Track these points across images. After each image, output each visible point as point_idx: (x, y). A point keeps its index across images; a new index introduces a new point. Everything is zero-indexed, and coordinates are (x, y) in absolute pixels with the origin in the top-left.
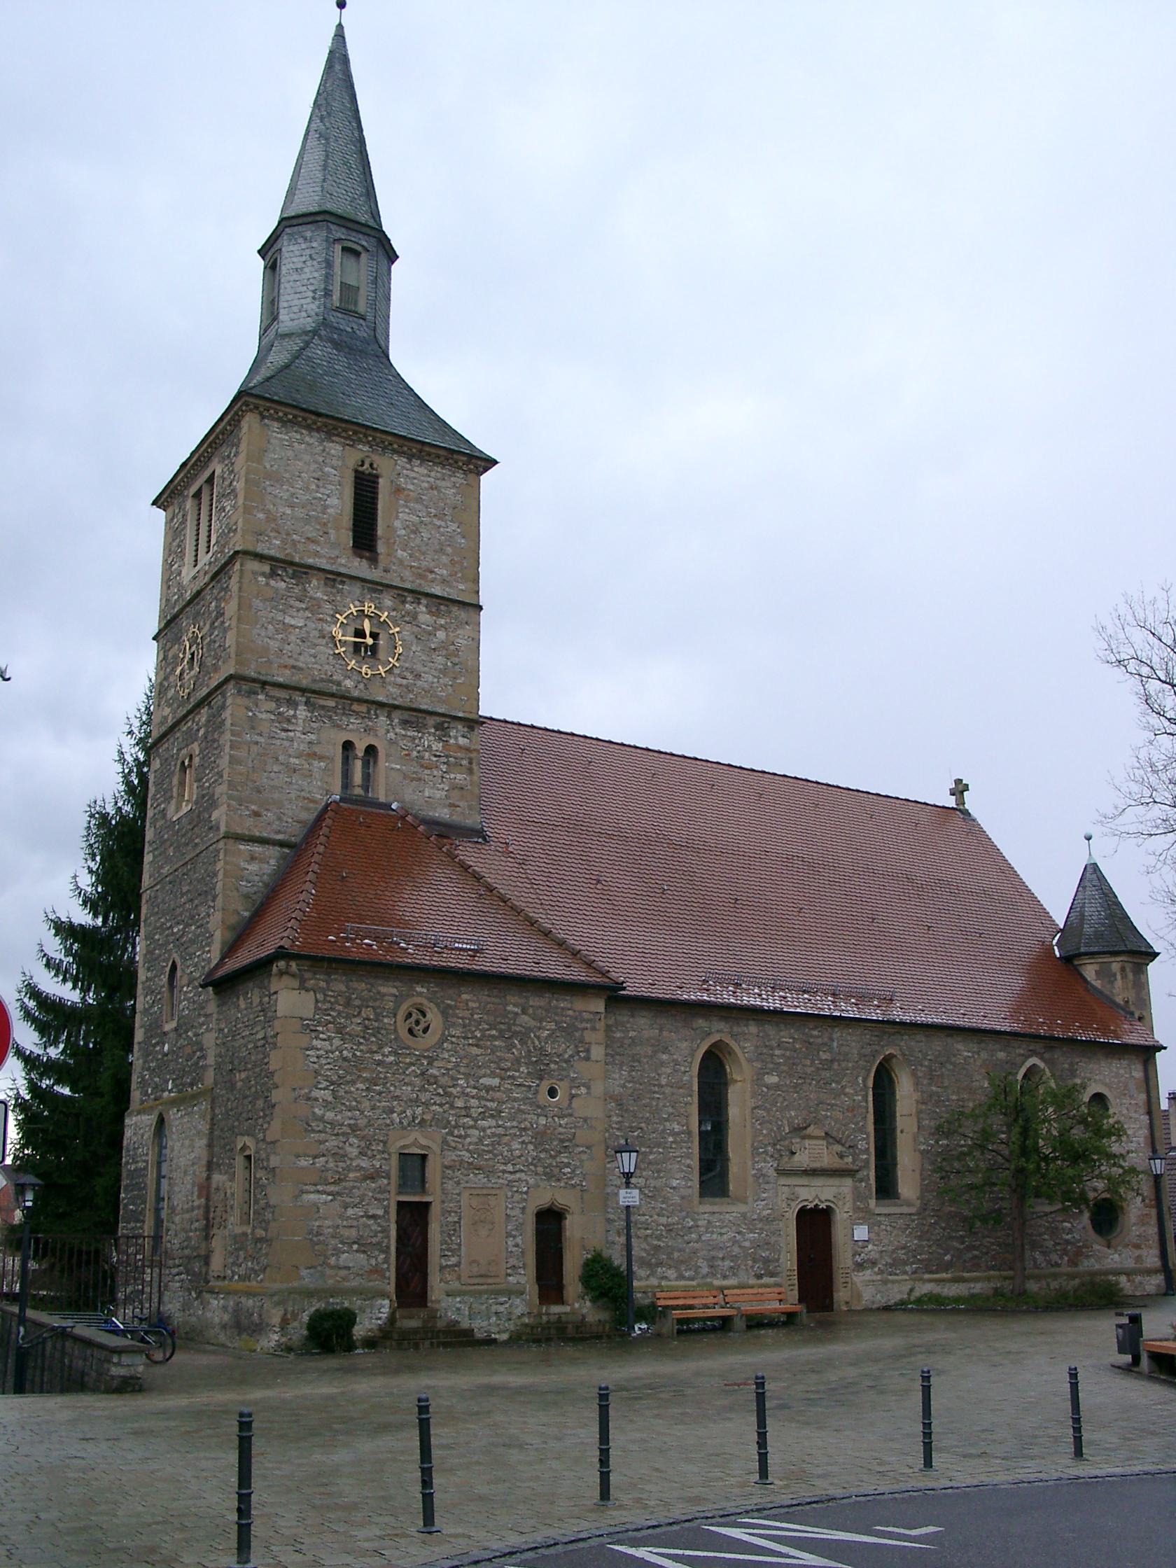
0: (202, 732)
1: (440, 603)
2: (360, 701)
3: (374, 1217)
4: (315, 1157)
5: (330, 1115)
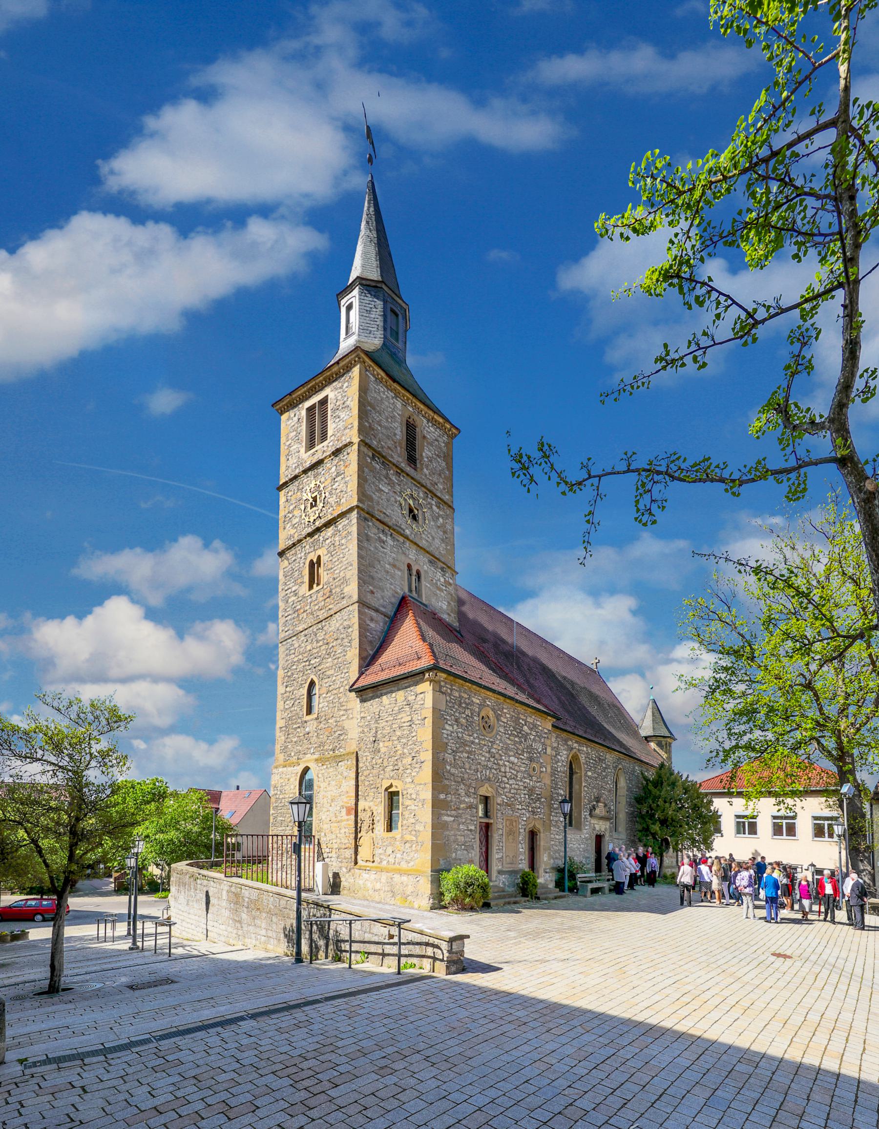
3: (471, 830)
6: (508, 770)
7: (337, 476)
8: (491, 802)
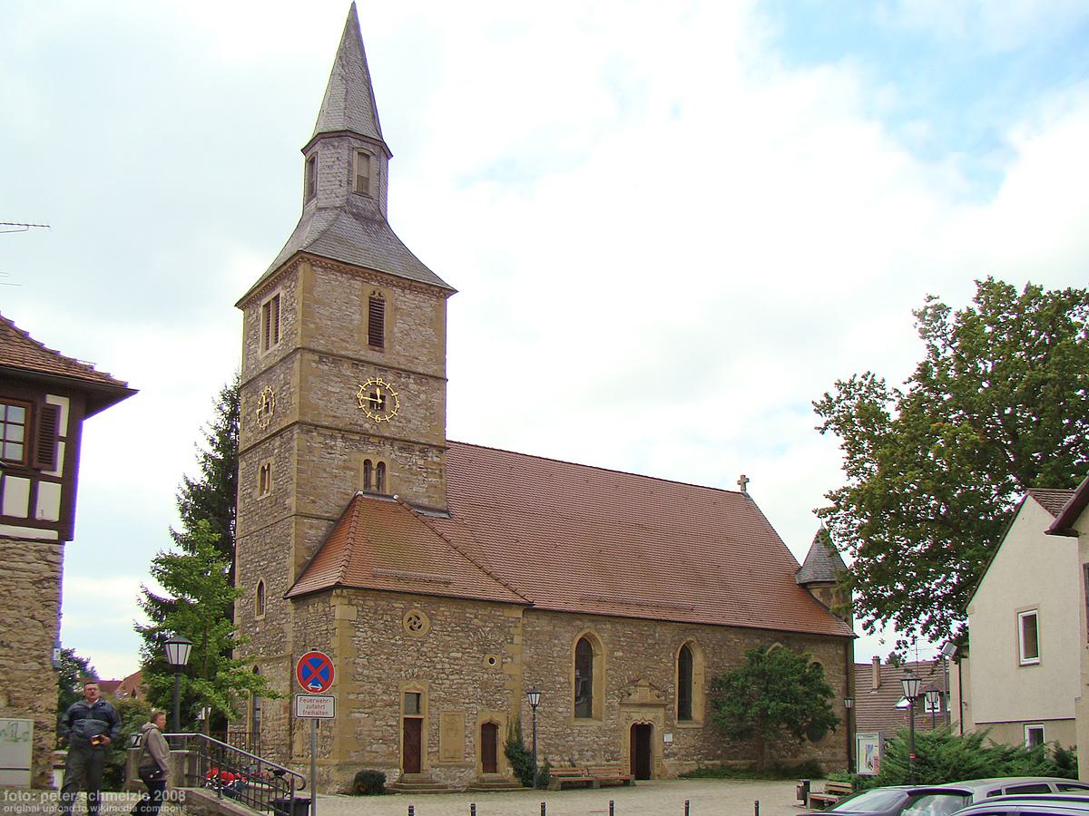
0: (276, 451)
1: (423, 377)
2: (374, 436)
3: (391, 726)
4: (358, 694)
5: (366, 672)
6: (447, 666)
7: (285, 385)
8: (422, 698)
